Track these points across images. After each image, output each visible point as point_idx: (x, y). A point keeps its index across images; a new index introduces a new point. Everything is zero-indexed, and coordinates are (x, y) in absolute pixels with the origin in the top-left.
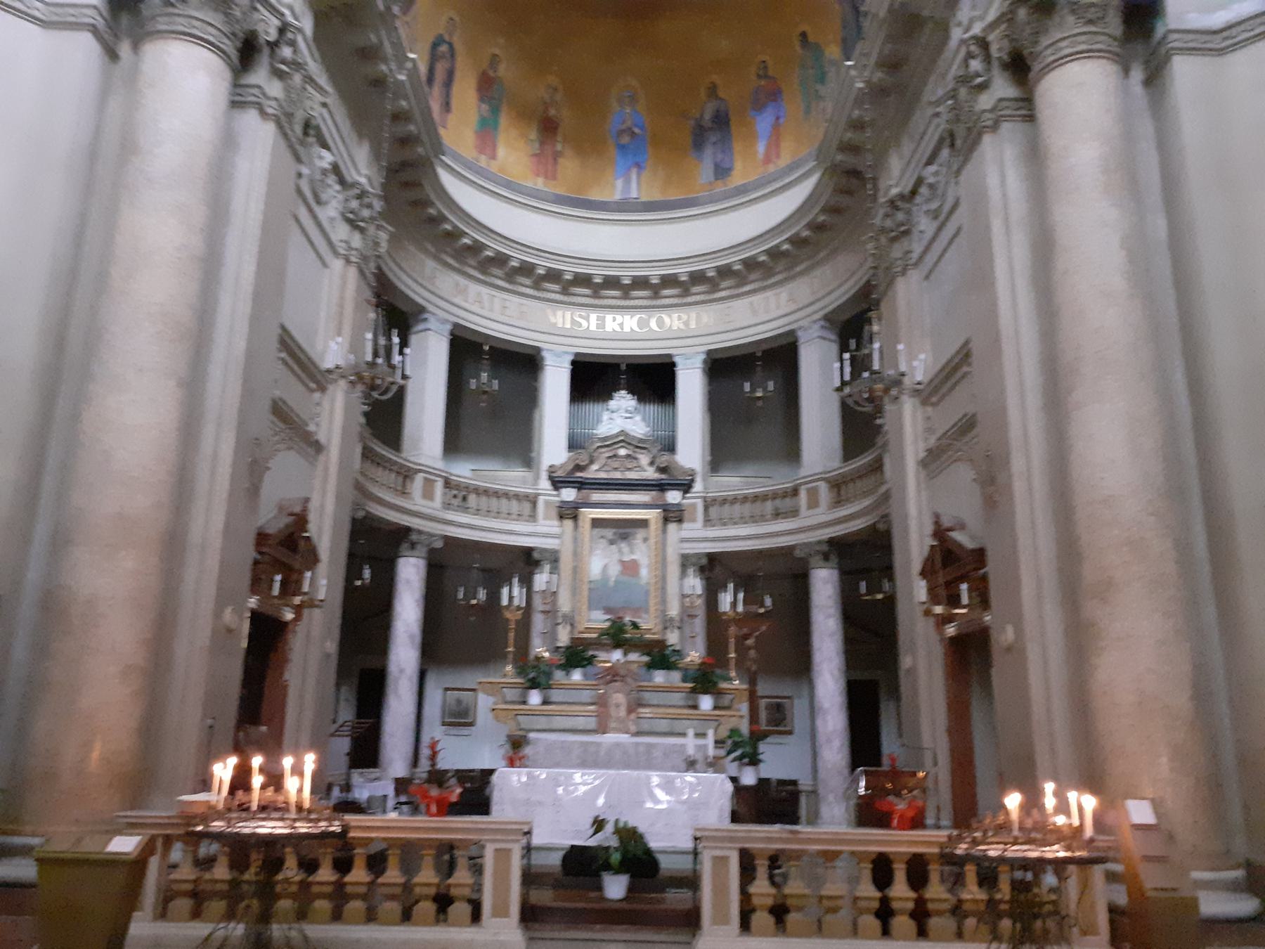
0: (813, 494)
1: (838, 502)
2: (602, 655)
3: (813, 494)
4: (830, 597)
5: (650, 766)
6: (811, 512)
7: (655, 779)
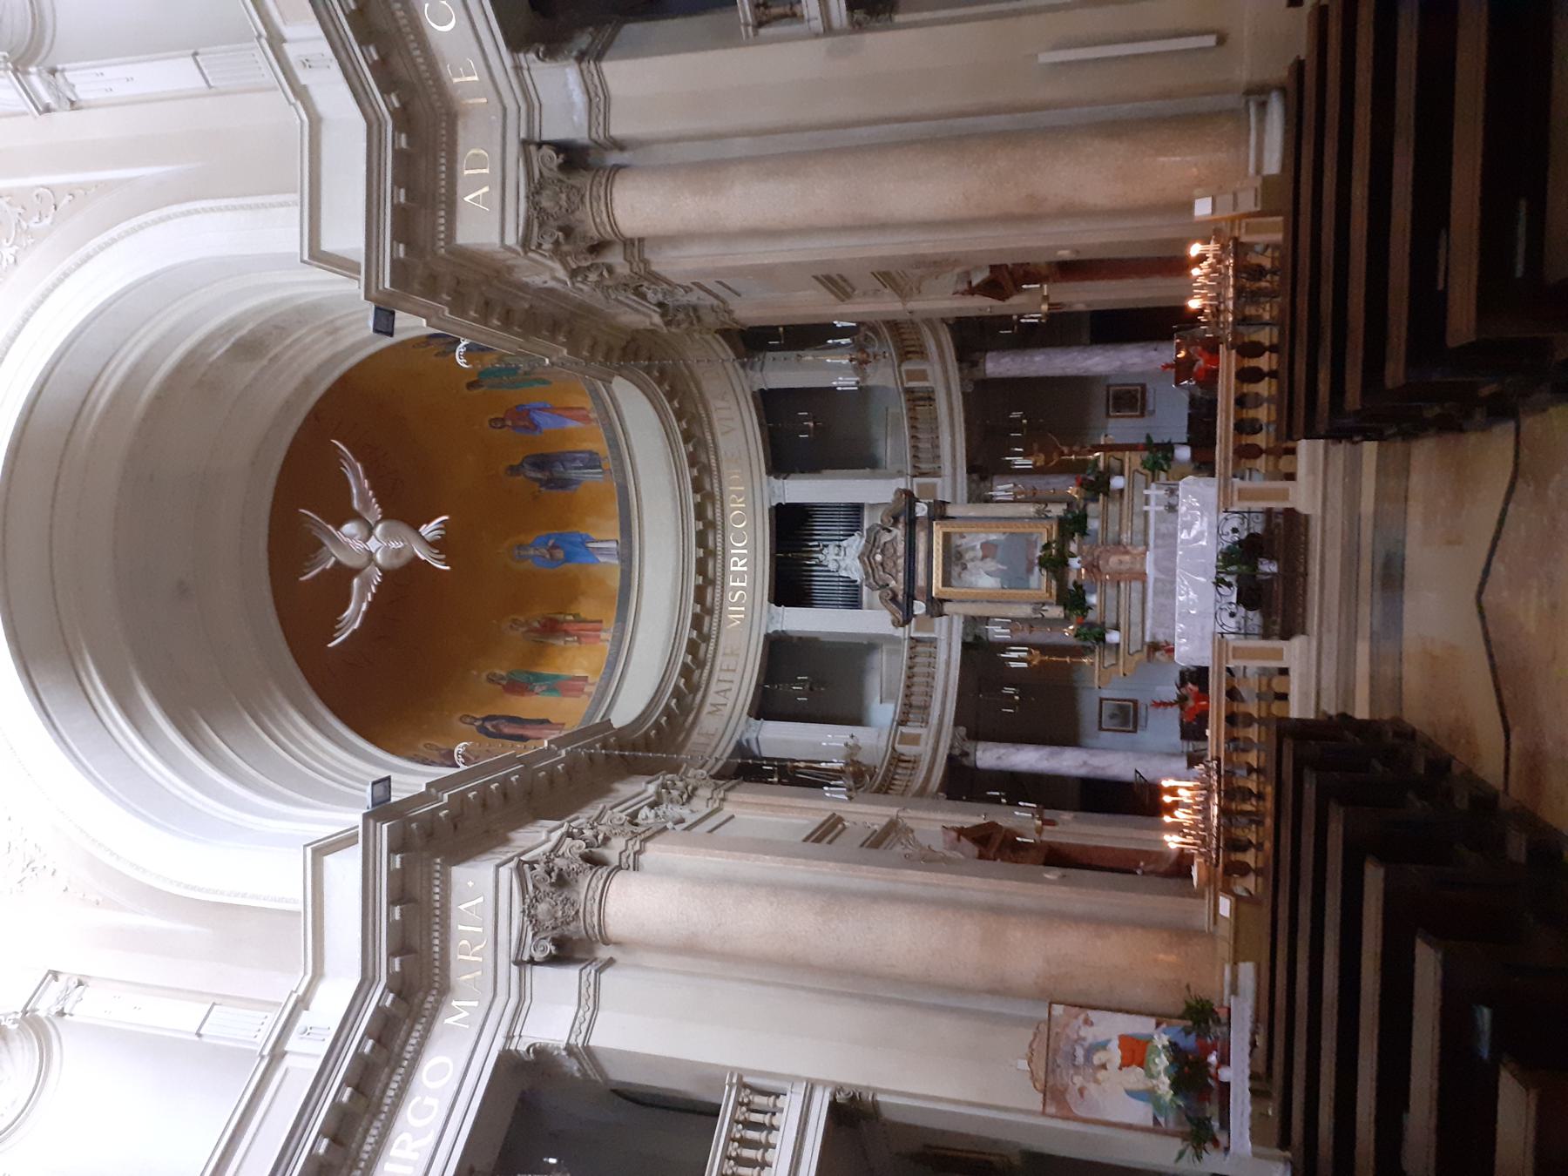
0: (912, 375)
1: (922, 353)
2: (1072, 577)
3: (912, 375)
4: (1013, 360)
5: (1174, 536)
6: (929, 378)
7: (1183, 536)
